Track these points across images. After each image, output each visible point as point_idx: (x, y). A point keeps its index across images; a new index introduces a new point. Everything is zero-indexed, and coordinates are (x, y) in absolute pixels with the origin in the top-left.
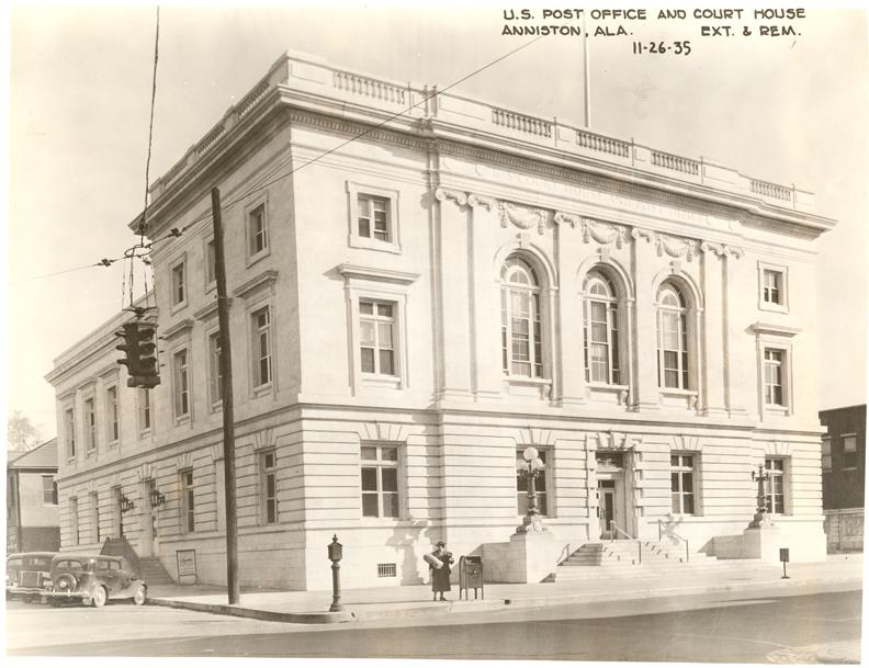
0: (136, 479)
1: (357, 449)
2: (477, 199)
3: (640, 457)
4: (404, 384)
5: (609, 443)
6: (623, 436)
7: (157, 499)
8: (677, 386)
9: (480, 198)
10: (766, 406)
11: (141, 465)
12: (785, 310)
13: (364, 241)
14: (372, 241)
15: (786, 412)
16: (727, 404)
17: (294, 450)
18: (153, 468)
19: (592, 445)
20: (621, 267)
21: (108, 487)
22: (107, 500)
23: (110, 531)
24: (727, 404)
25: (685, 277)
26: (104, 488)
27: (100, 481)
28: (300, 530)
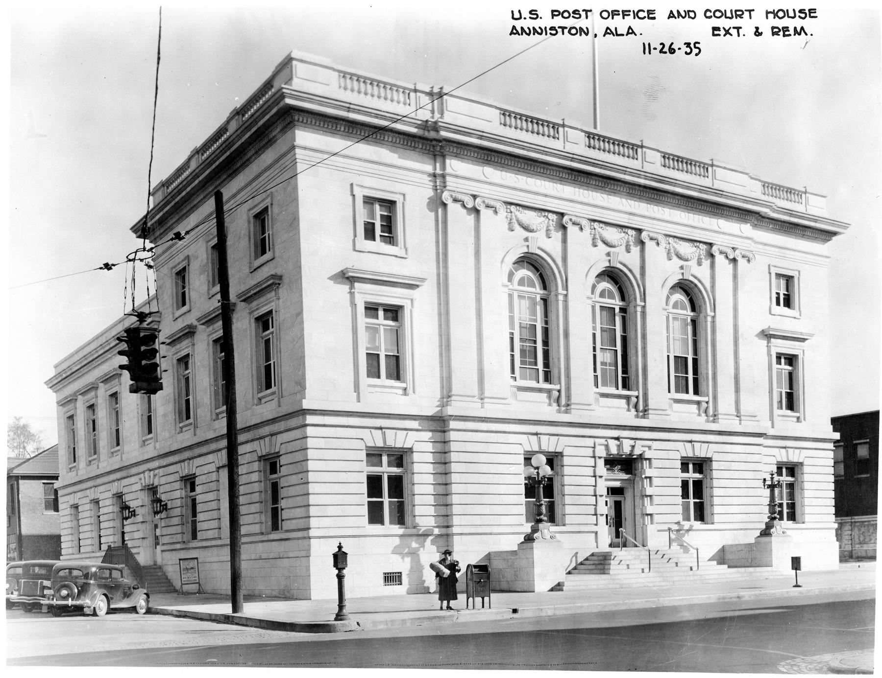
0: (138, 487)
1: (363, 455)
2: (484, 202)
3: (650, 464)
4: (410, 390)
5: (619, 450)
6: (632, 442)
7: (159, 506)
8: (687, 392)
9: (487, 201)
10: (777, 412)
11: (144, 472)
12: (402, 253)
13: (370, 245)
14: (378, 245)
15: (798, 418)
16: (738, 409)
17: (298, 457)
18: (155, 476)
19: (601, 452)
20: (630, 271)
21: (109, 494)
22: (109, 507)
23: (111, 539)
24: (738, 409)
25: (696, 282)
26: (106, 495)
27: (102, 488)
28: (304, 538)
